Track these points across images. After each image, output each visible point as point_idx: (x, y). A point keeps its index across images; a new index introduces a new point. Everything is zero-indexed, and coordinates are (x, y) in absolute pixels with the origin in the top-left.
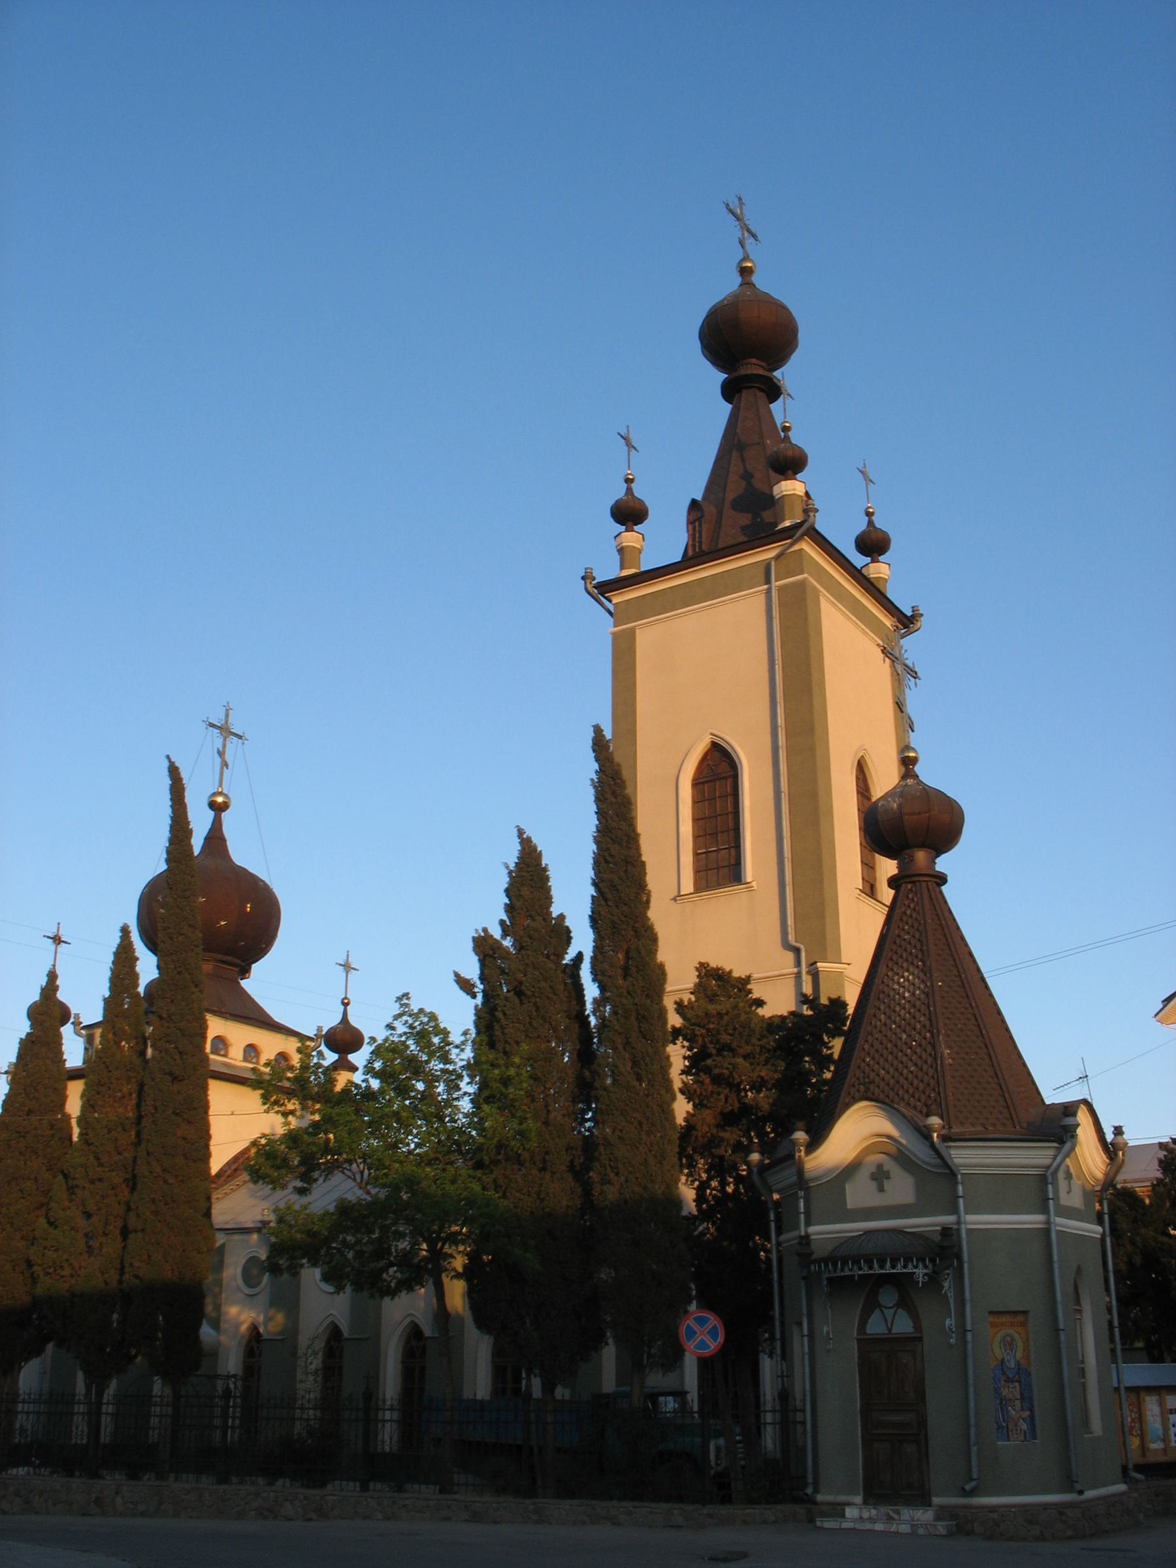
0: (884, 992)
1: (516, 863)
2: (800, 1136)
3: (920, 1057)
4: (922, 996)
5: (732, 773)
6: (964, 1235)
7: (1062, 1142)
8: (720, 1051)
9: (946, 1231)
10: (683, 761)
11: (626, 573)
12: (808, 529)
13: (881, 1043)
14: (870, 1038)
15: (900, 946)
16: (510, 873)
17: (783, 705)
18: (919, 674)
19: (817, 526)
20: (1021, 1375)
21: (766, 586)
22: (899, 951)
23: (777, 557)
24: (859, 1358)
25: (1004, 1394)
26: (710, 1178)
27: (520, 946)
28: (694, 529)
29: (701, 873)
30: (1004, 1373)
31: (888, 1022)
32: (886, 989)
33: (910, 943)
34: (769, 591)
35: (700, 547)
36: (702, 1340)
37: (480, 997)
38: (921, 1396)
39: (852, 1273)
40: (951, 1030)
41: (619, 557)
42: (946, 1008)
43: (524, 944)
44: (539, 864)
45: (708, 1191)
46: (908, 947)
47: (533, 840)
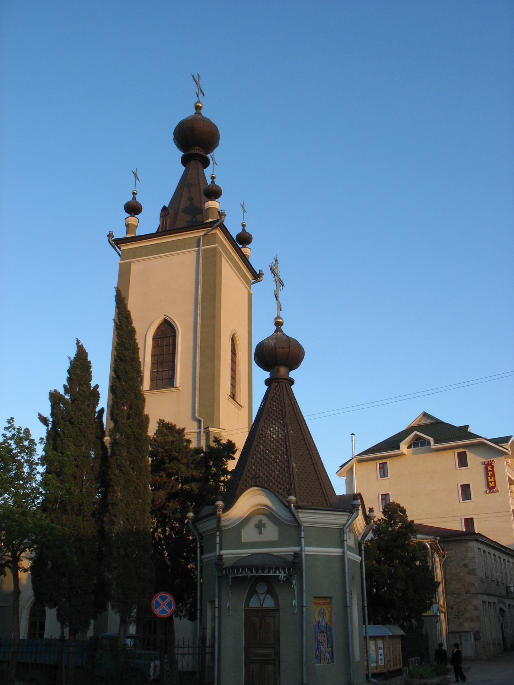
0: (262, 435)
1: (74, 357)
2: (220, 503)
3: (281, 468)
4: (282, 437)
5: (173, 335)
6: (304, 557)
7: (352, 512)
8: (171, 461)
9: (297, 555)
10: (148, 329)
11: (129, 236)
12: (220, 224)
13: (261, 460)
14: (255, 457)
15: (271, 413)
16: (71, 362)
17: (201, 304)
18: (284, 284)
19: (224, 223)
20: (327, 630)
21: (197, 248)
22: (271, 415)
23: (204, 235)
24: (245, 620)
25: (319, 639)
26: (158, 528)
27: (74, 400)
28: (163, 220)
29: (154, 381)
30: (319, 628)
31: (265, 449)
32: (263, 433)
33: (276, 411)
34: (198, 251)
35: (166, 227)
36: (163, 608)
37: (50, 426)
38: (278, 640)
39: (247, 575)
40: (297, 455)
41: (126, 229)
42: (294, 444)
43: (76, 398)
44: (86, 359)
45: (156, 534)
46: (275, 413)
47: (84, 346)
